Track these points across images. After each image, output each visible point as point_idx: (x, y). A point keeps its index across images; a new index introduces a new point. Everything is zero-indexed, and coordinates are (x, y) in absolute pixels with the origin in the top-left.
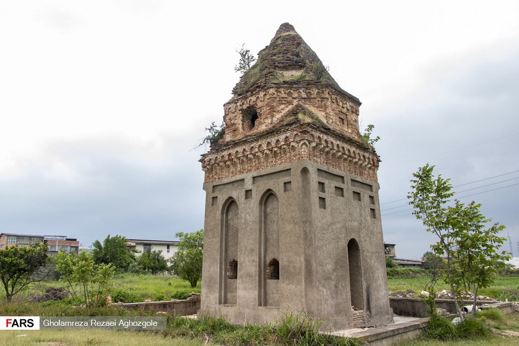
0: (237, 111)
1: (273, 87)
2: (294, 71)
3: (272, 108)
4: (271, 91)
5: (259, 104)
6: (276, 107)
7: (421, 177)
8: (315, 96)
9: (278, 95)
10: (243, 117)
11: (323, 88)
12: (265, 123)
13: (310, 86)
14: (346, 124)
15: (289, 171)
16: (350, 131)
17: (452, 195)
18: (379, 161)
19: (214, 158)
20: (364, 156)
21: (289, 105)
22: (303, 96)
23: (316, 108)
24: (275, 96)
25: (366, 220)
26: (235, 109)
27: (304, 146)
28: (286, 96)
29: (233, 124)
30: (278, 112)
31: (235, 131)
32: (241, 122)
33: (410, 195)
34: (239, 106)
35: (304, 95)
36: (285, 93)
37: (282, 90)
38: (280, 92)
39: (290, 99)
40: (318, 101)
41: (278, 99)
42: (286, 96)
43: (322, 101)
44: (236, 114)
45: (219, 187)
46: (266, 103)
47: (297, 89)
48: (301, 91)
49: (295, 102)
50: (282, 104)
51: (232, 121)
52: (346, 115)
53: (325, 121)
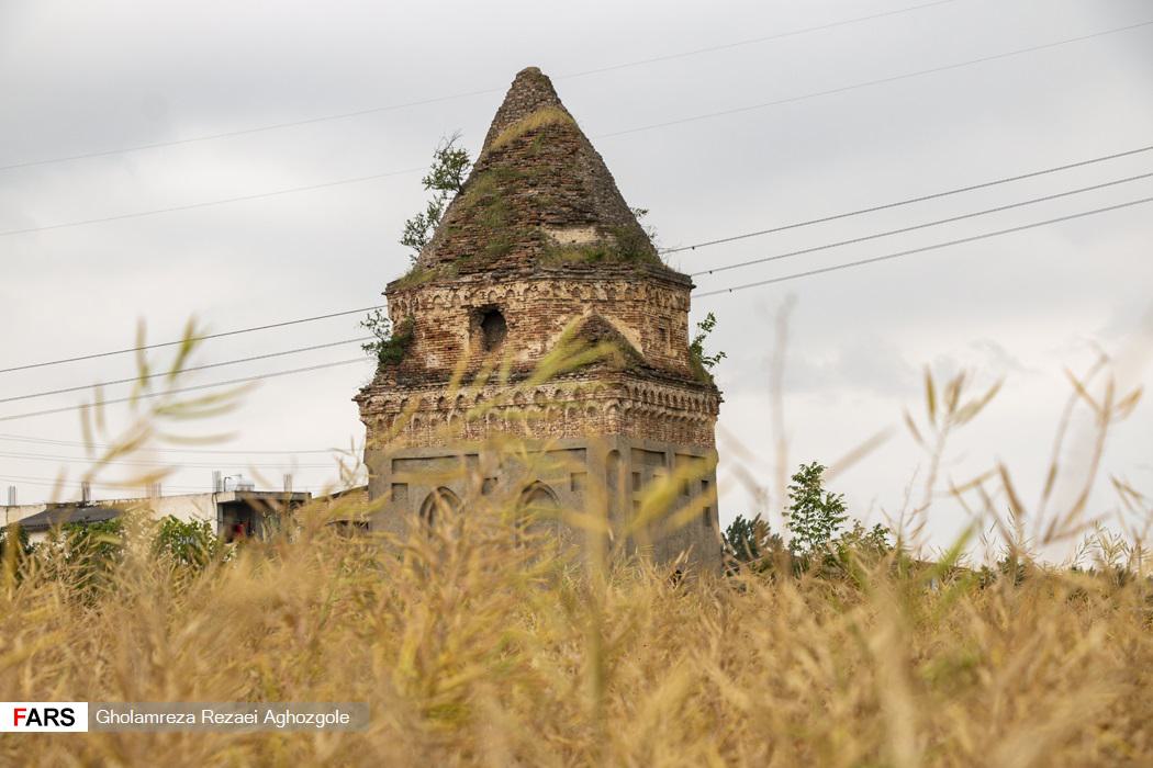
0: (458, 308)
1: (546, 279)
2: (576, 230)
3: (544, 319)
4: (542, 286)
5: (514, 306)
6: (550, 320)
7: (803, 481)
8: (623, 298)
9: (555, 295)
10: (470, 321)
11: (637, 281)
12: (526, 347)
13: (614, 277)
14: (668, 340)
15: (581, 452)
16: (675, 354)
17: (846, 518)
18: (720, 401)
19: (400, 402)
20: (697, 401)
21: (576, 314)
22: (602, 298)
23: (623, 322)
24: (550, 296)
25: (696, 533)
26: (452, 302)
27: (613, 410)
28: (569, 296)
29: (446, 334)
30: (557, 329)
31: (450, 349)
32: (468, 334)
33: (787, 511)
34: (462, 298)
35: (602, 295)
36: (568, 291)
37: (562, 284)
38: (559, 288)
39: (577, 302)
40: (628, 306)
41: (554, 302)
42: (569, 296)
43: (634, 307)
44: (452, 312)
45: (409, 463)
46: (528, 307)
47: (590, 284)
48: (598, 286)
49: (587, 312)
50: (563, 312)
51: (442, 327)
52: (670, 320)
53: (639, 349)
